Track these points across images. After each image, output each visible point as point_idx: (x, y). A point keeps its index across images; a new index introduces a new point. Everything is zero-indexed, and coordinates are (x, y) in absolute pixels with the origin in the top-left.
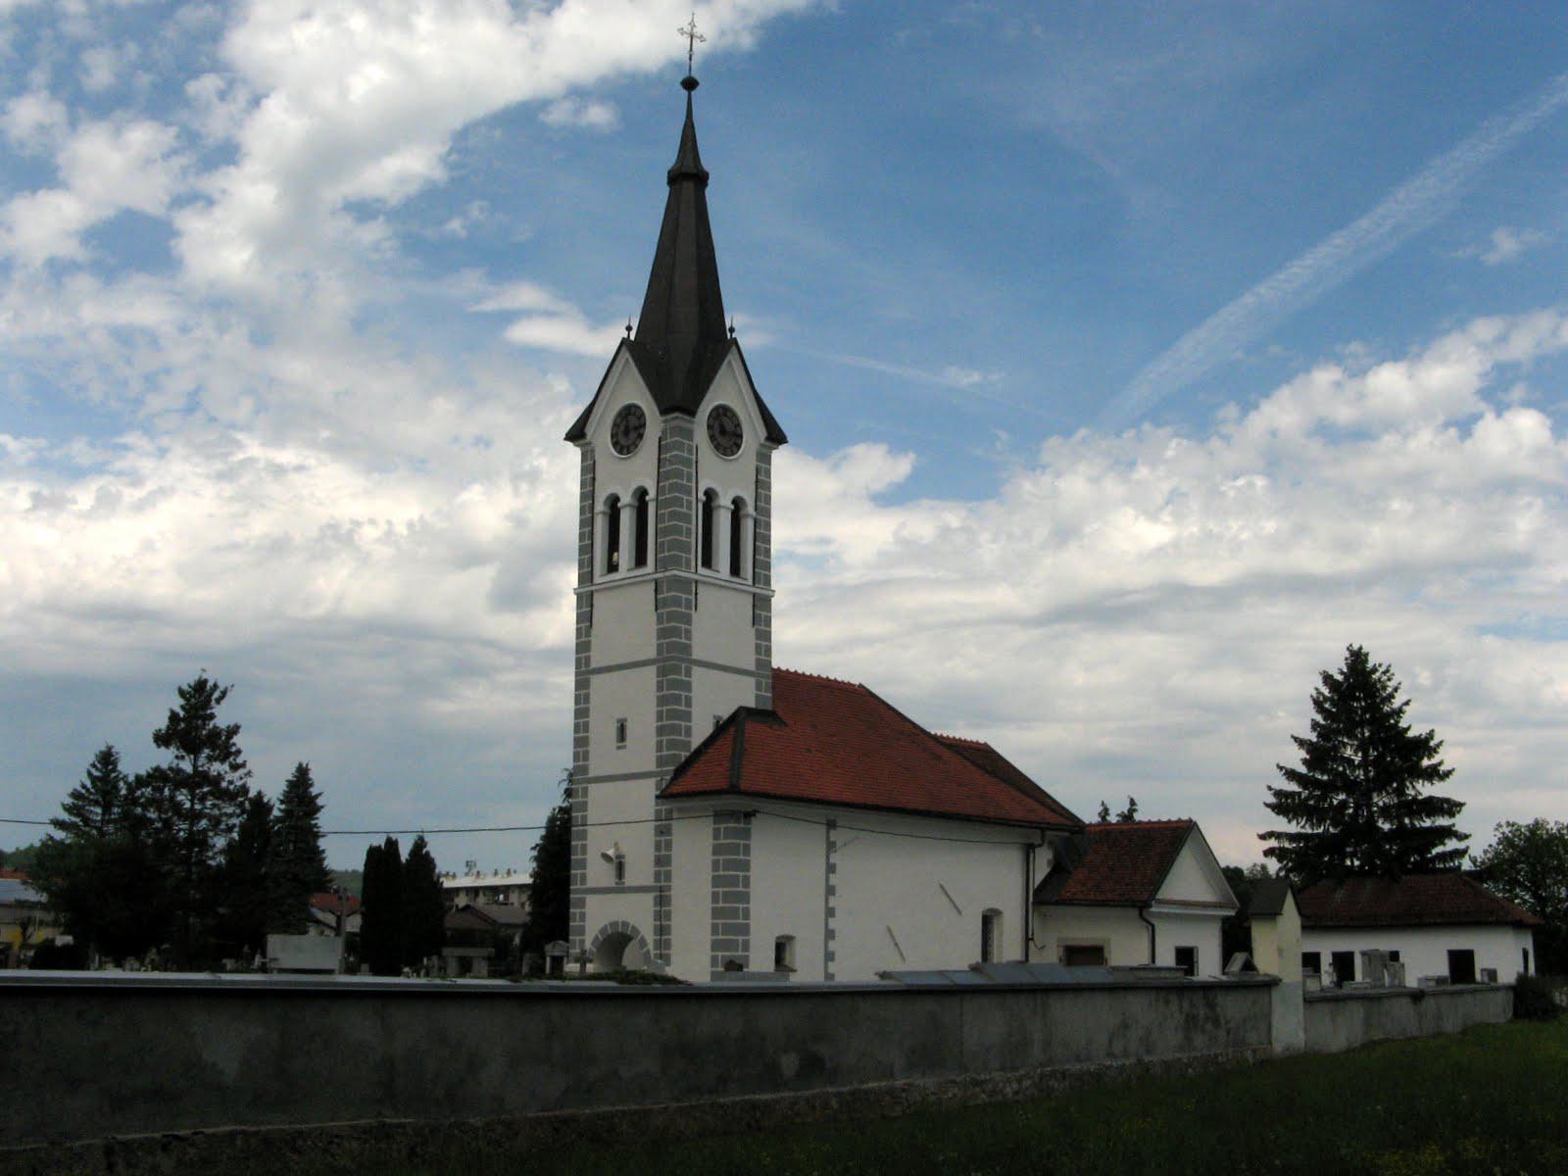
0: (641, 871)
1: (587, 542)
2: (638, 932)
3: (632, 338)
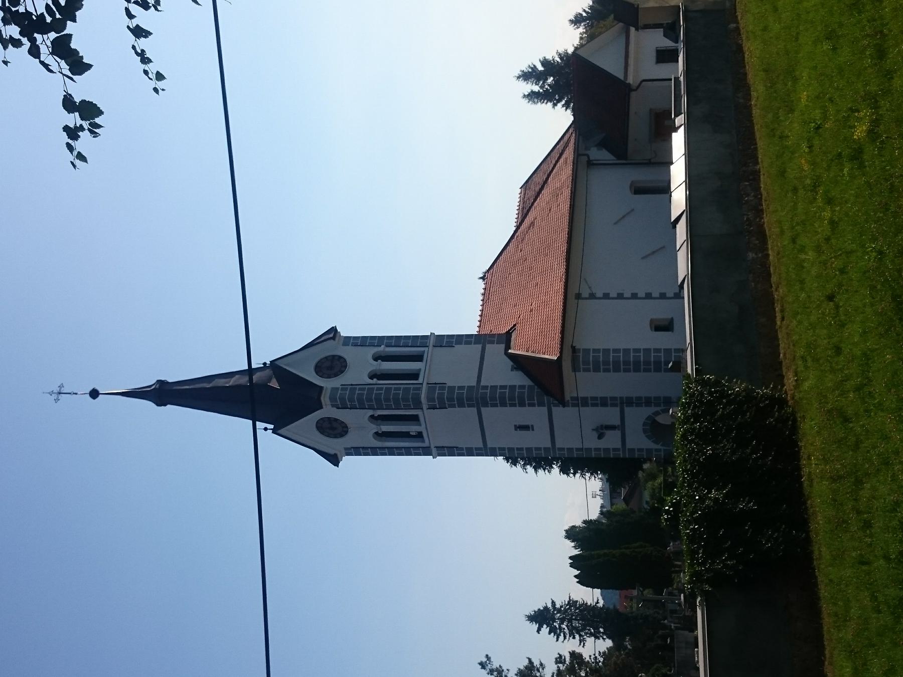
0: (611, 415)
1: (369, 450)
3: (272, 426)
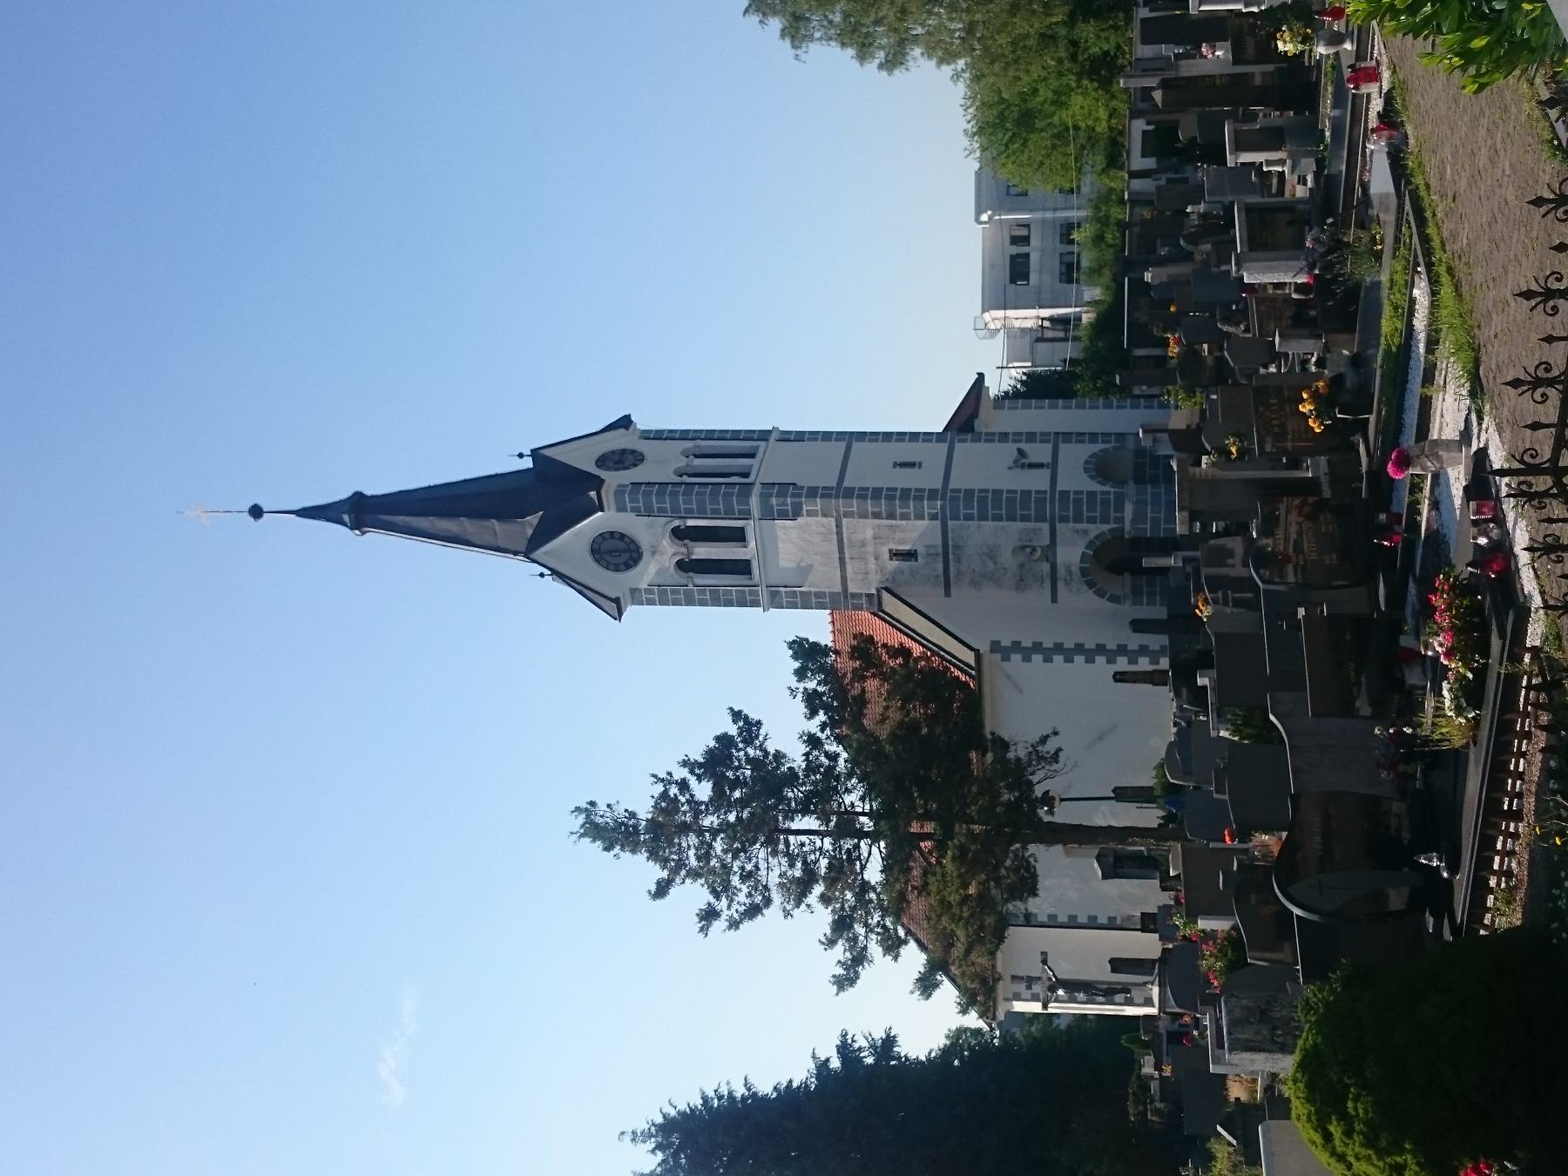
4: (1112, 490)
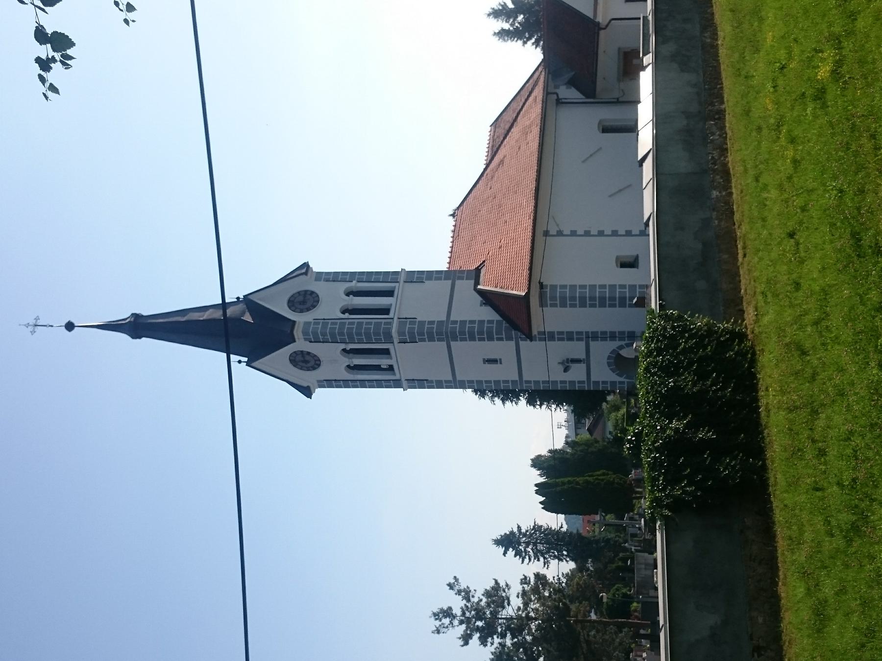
0: (577, 349)
1: (358, 383)
2: (614, 350)
3: (246, 359)
4: (626, 380)
